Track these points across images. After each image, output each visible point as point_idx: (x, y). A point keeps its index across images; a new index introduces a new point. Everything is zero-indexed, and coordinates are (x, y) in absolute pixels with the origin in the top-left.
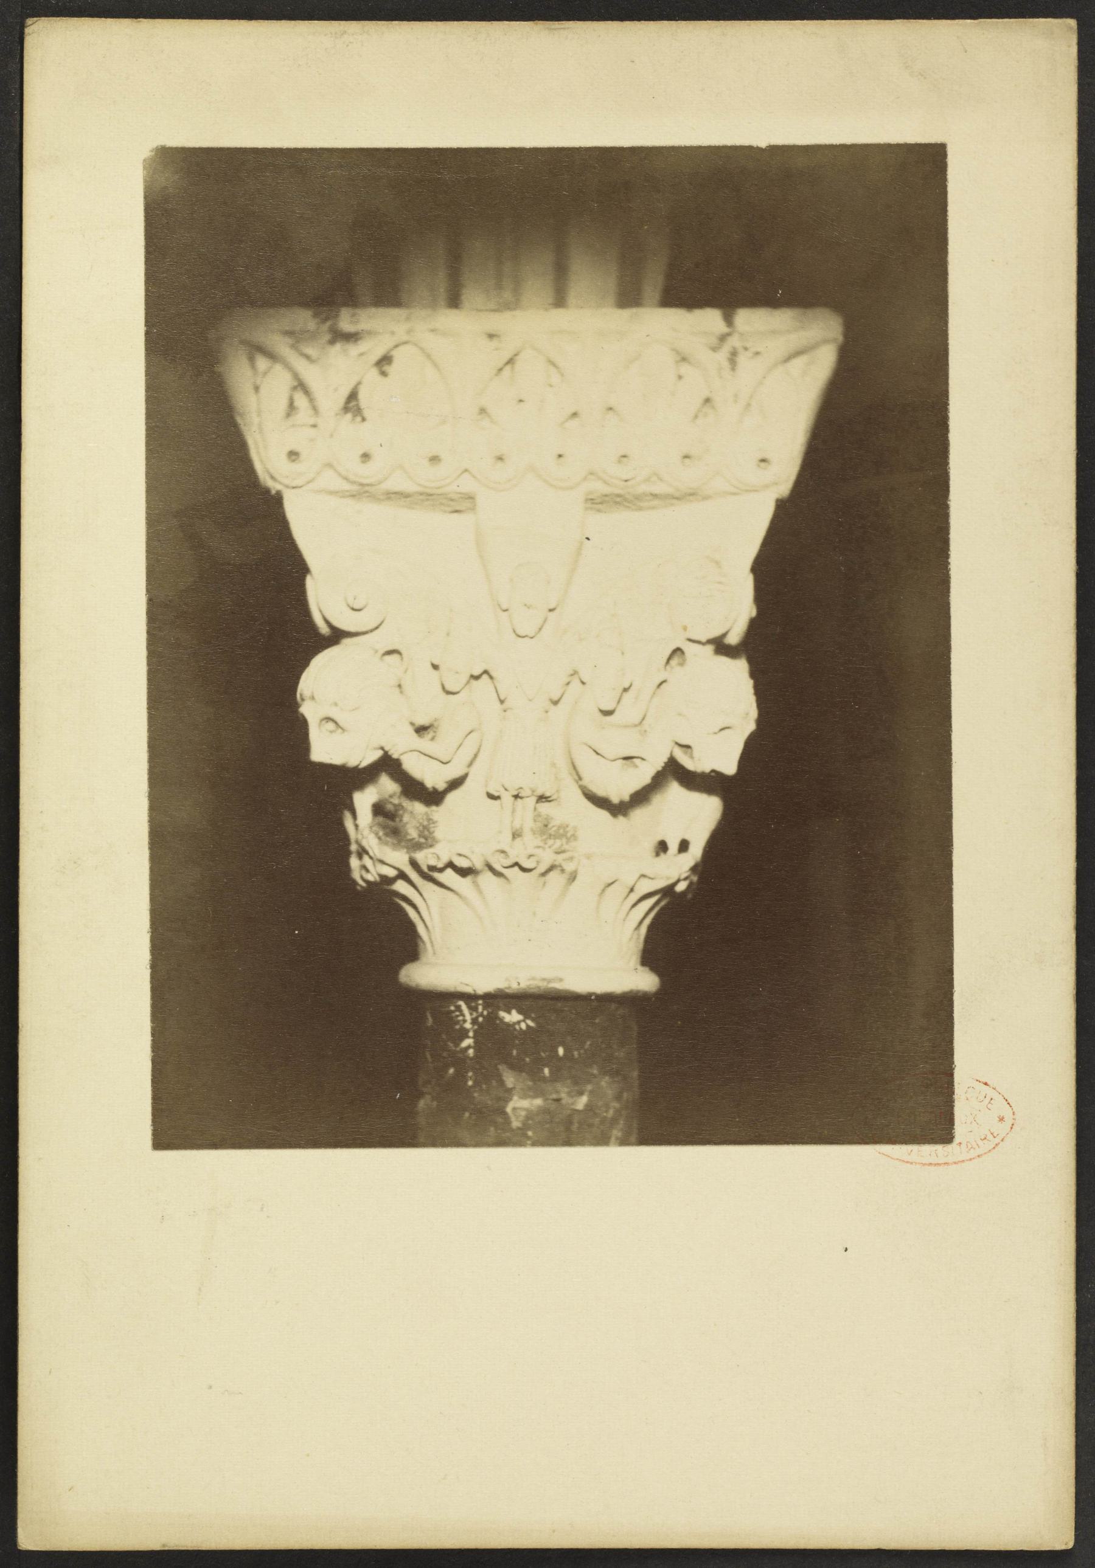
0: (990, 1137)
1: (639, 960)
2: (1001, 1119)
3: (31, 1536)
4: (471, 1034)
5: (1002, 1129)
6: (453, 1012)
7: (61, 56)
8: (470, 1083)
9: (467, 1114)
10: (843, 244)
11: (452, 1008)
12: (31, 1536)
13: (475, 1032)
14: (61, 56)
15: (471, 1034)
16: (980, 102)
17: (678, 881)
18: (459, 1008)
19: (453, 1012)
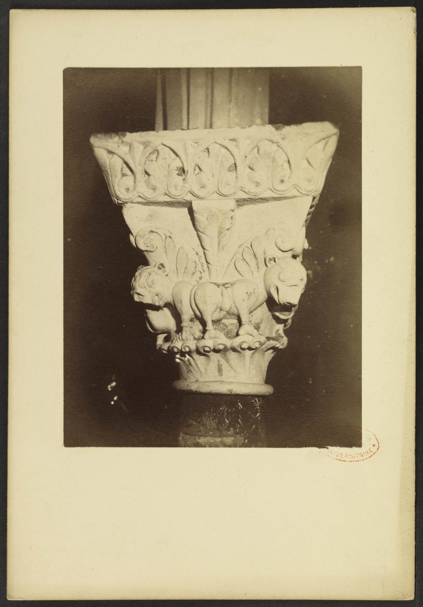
0: (369, 452)
1: (264, 380)
2: (374, 446)
3: (410, 597)
4: (259, 411)
5: (374, 449)
6: (254, 402)
7: (24, 24)
8: (260, 430)
9: (259, 443)
10: (301, 97)
11: (253, 401)
12: (410, 597)
13: (260, 409)
14: (24, 24)
15: (259, 411)
16: (366, 44)
17: (207, 347)
18: (255, 401)
19: (254, 402)
